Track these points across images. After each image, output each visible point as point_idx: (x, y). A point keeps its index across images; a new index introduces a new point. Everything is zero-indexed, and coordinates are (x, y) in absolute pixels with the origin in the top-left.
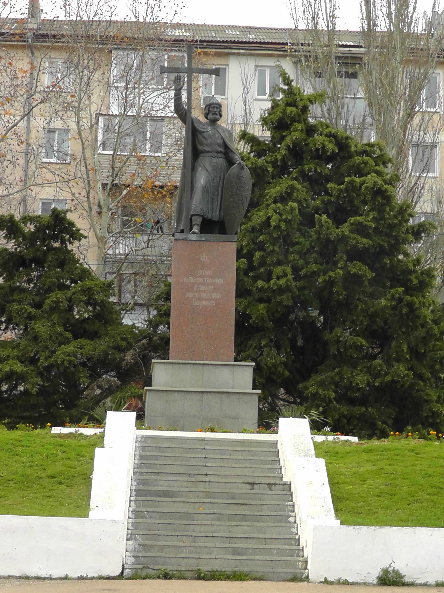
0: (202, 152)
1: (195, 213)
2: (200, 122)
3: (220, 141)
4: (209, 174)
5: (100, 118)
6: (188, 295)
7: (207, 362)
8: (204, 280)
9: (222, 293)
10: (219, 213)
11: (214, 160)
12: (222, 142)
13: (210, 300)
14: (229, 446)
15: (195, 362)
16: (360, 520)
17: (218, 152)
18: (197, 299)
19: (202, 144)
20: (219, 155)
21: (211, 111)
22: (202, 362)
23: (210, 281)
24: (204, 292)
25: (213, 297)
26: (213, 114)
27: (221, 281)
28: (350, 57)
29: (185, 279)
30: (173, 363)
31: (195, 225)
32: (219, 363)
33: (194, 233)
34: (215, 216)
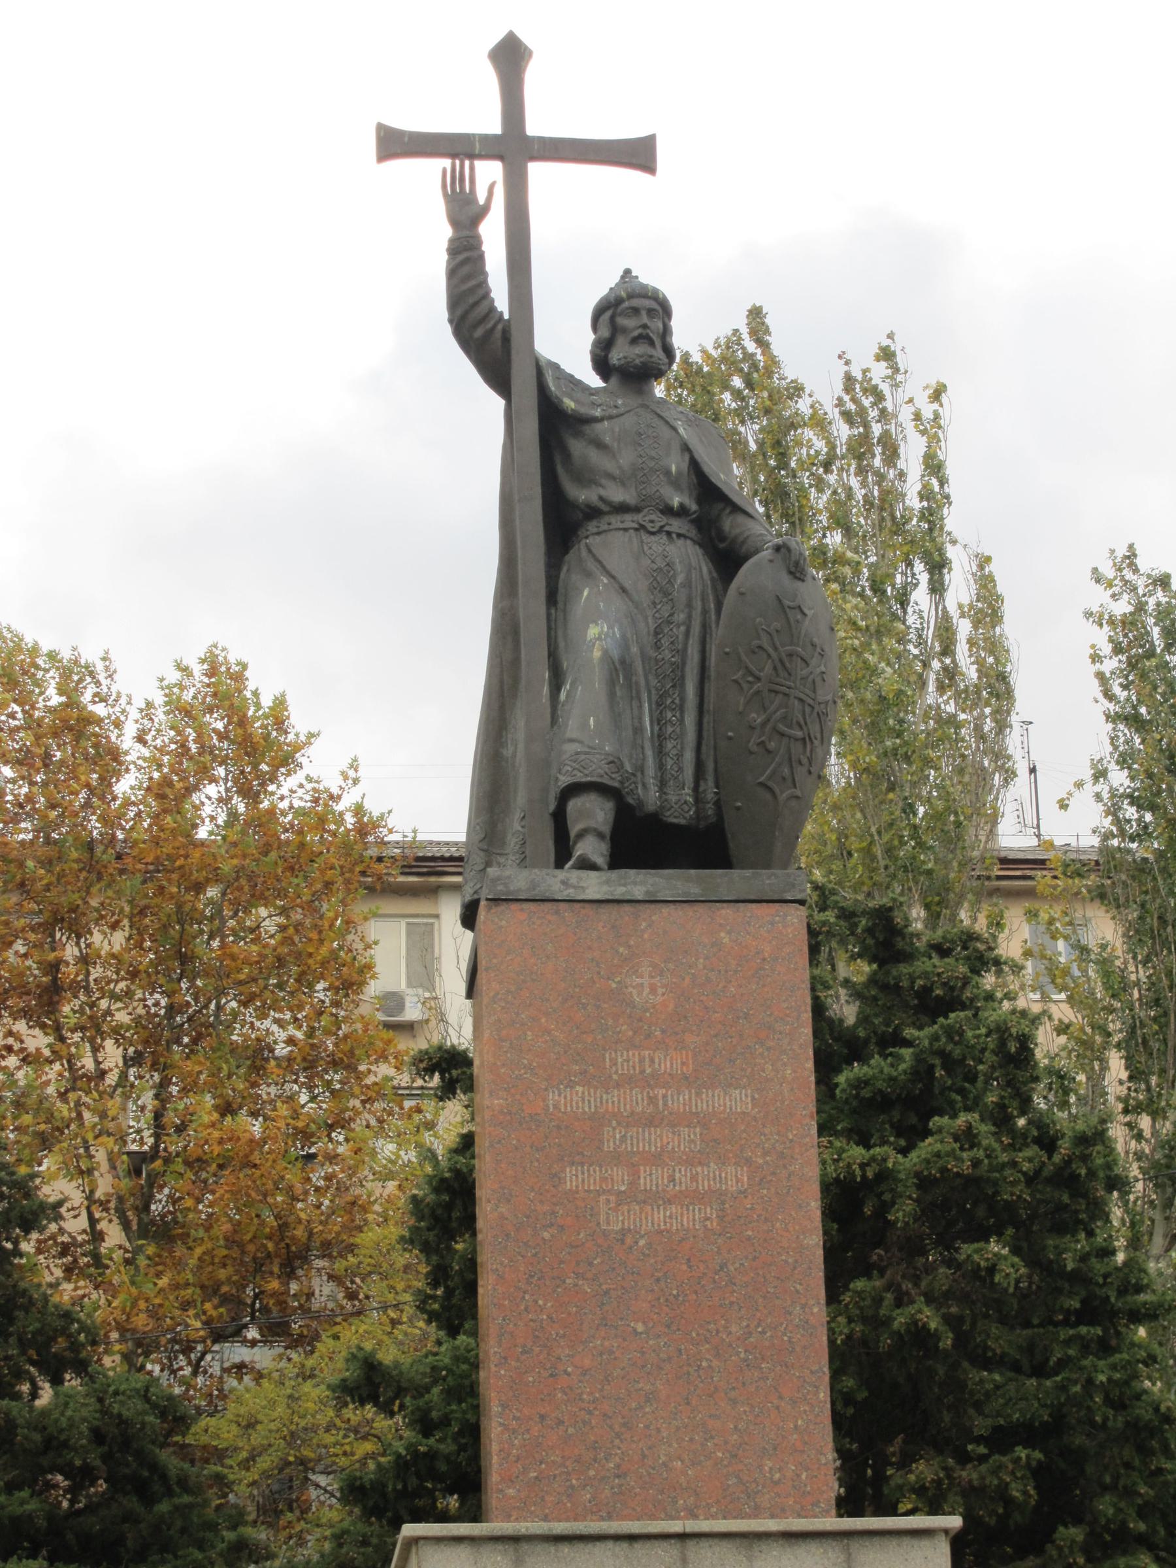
0: (593, 513)
1: (580, 777)
2: (575, 384)
3: (676, 464)
4: (637, 605)
6: (572, 1178)
7: (705, 1526)
8: (652, 1100)
9: (748, 1161)
10: (696, 788)
11: (657, 545)
12: (685, 466)
13: (696, 1197)
14: (567, 1520)
15: (635, 1527)
17: (668, 511)
18: (623, 1198)
19: (585, 478)
20: (676, 525)
21: (624, 330)
22: (676, 1527)
23: (680, 1101)
24: (656, 1159)
26: (634, 341)
27: (739, 1101)
29: (552, 1097)
30: (515, 1539)
31: (581, 835)
32: (772, 1525)
33: (586, 865)
34: (675, 800)
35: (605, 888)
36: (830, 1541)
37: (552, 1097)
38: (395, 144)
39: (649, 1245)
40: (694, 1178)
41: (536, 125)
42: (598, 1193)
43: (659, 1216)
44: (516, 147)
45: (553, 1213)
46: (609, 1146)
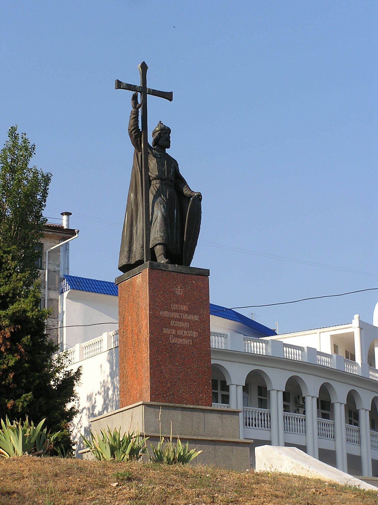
6: (165, 331)
7: (188, 406)
8: (180, 316)
9: (198, 331)
13: (187, 337)
23: (185, 316)
24: (181, 328)
25: (189, 335)
29: (161, 313)
37: (161, 313)
38: (119, 85)
39: (179, 347)
40: (188, 333)
41: (149, 86)
42: (170, 334)
44: (144, 90)
46: (172, 325)
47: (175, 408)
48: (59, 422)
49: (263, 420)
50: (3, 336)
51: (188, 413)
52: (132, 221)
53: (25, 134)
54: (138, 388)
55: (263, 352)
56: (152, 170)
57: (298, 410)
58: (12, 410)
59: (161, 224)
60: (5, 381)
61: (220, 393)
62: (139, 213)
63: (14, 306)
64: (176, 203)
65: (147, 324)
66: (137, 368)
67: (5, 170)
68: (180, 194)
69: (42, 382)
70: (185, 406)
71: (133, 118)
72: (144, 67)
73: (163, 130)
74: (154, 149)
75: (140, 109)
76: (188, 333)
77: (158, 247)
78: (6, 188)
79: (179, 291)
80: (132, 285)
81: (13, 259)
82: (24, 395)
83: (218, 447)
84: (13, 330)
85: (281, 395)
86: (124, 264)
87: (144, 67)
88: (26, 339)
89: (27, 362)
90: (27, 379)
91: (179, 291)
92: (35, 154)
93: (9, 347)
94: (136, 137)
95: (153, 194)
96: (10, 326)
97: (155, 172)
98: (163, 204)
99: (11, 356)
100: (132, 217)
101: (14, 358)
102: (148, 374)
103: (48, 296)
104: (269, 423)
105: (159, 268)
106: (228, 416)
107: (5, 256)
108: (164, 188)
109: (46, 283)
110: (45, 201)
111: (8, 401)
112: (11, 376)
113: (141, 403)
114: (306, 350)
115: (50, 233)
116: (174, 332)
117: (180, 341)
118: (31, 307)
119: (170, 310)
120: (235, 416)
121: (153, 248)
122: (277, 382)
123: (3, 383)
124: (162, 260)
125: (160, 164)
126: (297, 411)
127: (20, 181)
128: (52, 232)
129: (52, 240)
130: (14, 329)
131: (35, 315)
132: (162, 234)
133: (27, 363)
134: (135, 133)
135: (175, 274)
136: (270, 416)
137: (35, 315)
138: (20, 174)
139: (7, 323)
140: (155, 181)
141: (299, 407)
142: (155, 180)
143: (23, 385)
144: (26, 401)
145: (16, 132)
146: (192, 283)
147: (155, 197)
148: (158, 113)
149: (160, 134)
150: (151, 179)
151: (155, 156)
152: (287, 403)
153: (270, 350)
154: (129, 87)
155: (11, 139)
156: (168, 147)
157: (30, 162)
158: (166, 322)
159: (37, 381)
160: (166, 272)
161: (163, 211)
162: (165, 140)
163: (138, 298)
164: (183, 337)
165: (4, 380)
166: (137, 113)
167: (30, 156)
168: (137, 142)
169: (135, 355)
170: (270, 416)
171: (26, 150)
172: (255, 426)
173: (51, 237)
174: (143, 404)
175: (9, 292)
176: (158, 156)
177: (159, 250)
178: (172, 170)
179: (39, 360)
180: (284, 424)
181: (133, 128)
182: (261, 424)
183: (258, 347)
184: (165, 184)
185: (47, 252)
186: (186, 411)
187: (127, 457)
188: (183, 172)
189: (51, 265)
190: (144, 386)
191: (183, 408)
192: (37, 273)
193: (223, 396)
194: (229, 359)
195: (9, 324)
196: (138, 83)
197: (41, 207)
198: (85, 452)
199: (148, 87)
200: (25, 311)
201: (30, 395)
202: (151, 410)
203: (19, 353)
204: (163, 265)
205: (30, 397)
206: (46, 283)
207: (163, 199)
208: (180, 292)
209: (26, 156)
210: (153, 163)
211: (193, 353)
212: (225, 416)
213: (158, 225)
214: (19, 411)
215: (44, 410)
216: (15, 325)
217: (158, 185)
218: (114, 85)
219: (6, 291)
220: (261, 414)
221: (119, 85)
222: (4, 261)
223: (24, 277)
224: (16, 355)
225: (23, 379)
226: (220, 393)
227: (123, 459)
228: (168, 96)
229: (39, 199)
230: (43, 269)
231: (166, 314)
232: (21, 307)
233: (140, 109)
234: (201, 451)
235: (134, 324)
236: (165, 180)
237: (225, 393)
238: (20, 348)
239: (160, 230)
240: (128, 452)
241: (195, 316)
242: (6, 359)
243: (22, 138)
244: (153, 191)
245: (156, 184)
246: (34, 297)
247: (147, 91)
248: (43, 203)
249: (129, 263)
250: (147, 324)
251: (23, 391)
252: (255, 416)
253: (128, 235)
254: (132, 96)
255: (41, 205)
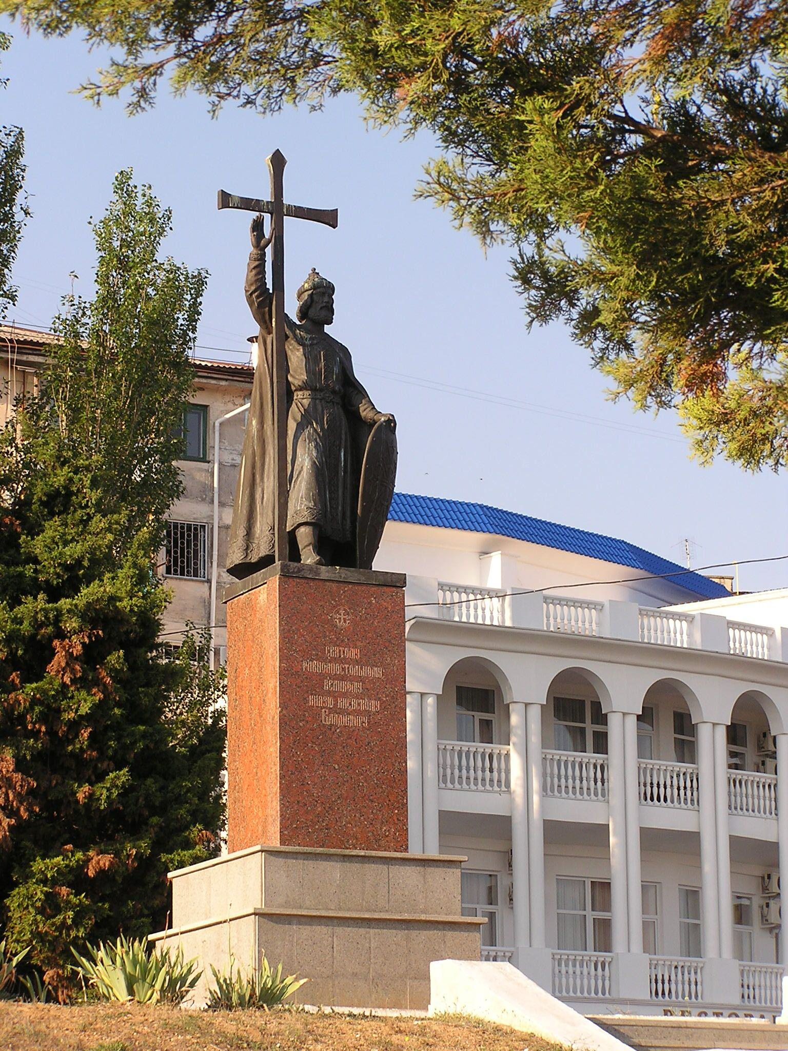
5: (189, 416)
6: (312, 701)
8: (343, 669)
13: (358, 713)
16: (381, 577)
23: (355, 670)
24: (344, 695)
28: (645, 910)
29: (305, 664)
35: (327, 574)
36: (311, 859)
37: (305, 664)
39: (341, 732)
40: (359, 704)
41: (288, 199)
43: (345, 719)
44: (278, 209)
45: (304, 715)
47: (328, 857)
48: (187, 827)
49: (682, 788)
50: (67, 652)
51: (356, 866)
52: (254, 475)
53: (150, 187)
54: (260, 814)
55: (682, 642)
56: (295, 371)
57: (763, 763)
58: (87, 806)
59: (309, 483)
60: (74, 745)
61: (590, 728)
62: (267, 460)
63: (90, 589)
64: (343, 437)
65: (275, 687)
66: (259, 774)
67: (108, 264)
68: (353, 416)
69: (152, 746)
70: (347, 852)
71: (254, 268)
72: (278, 161)
73: (318, 287)
74: (299, 327)
75: (268, 247)
76: (359, 704)
77: (302, 530)
78: (110, 303)
79: (342, 620)
80: (251, 606)
81: (94, 484)
82: (112, 775)
83: (414, 933)
84: (87, 640)
85: (721, 734)
86: (237, 562)
87: (278, 161)
88: (116, 658)
89: (119, 705)
90: (118, 739)
91: (342, 620)
92: (171, 229)
93: (79, 675)
94: (260, 305)
95: (295, 420)
96: (81, 631)
97: (302, 374)
98: (316, 440)
99: (83, 693)
100: (253, 467)
101: (90, 698)
102: (276, 788)
103: (220, 519)
104: (695, 793)
105: (300, 575)
106: (437, 870)
107: (76, 478)
108: (319, 408)
109: (216, 490)
110: (194, 330)
111: (80, 786)
112: (85, 735)
113: (258, 848)
114: (778, 634)
115: (223, 383)
116: (330, 702)
117: (344, 720)
118: (129, 588)
119: (323, 659)
120: (452, 870)
121: (294, 530)
122: (714, 705)
123: (70, 748)
124: (309, 557)
125: (310, 359)
126: (760, 767)
127: (139, 287)
128: (226, 380)
129: (227, 398)
130: (89, 637)
131: (136, 605)
132: (311, 504)
133: (119, 707)
134: (257, 297)
135: (334, 585)
136: (697, 779)
137: (136, 605)
138: (139, 273)
139: (74, 625)
140: (300, 393)
141: (767, 756)
142: (301, 390)
143: (110, 752)
144: (117, 786)
145: (131, 183)
146: (370, 603)
147: (300, 427)
148: (306, 253)
149: (311, 296)
150: (293, 388)
151: (301, 342)
152: (735, 748)
153: (698, 637)
154: (247, 204)
155: (120, 198)
156: (330, 322)
157: (159, 248)
158: (315, 684)
159: (141, 745)
160: (316, 582)
161: (315, 454)
162: (321, 308)
163: (261, 633)
164: (349, 712)
165: (71, 742)
166: (262, 258)
167: (160, 234)
168: (263, 314)
169: (255, 747)
170: (697, 779)
171: (152, 221)
172: (665, 800)
173: (224, 392)
174: (262, 851)
175: (83, 557)
176: (307, 342)
177: (304, 536)
178: (336, 370)
179: (146, 699)
180: (729, 795)
181: (253, 288)
182: (679, 795)
183: (680, 626)
184: (321, 400)
185: (217, 424)
186: (351, 862)
187: (156, 996)
188: (360, 374)
189: (226, 452)
190: (269, 811)
191: (344, 856)
192: (177, 486)
193: (595, 733)
194: (608, 657)
195: (80, 627)
196: (266, 195)
197: (186, 342)
198: (162, 938)
199: (286, 201)
200: (113, 599)
201: (123, 776)
202: (280, 861)
203: (101, 687)
204: (310, 568)
205: (123, 779)
206: (216, 490)
207: (315, 430)
208: (345, 622)
209: (150, 234)
210: (296, 356)
211: (369, 743)
212: (429, 870)
213: (304, 484)
214: (102, 807)
215: (157, 804)
216: (91, 630)
217: (306, 402)
218: (215, 200)
219: (76, 556)
220: (678, 775)
221: (226, 200)
222: (75, 489)
223: (117, 523)
224: (94, 690)
225: (110, 739)
226: (590, 728)
227: (149, 999)
228: (329, 218)
229: (182, 325)
230: (209, 462)
231: (313, 666)
232: (105, 590)
233: (268, 247)
234: (305, 980)
235: (253, 684)
236: (321, 390)
237: (599, 728)
238: (104, 677)
239: (308, 494)
240: (158, 986)
241: (375, 669)
242: (74, 701)
243: (144, 195)
244: (295, 414)
245: (302, 399)
246: (134, 568)
247: (285, 210)
248: (190, 334)
249: (248, 561)
250: (275, 687)
251: (112, 765)
252: (665, 778)
253: (246, 504)
254: (251, 222)
255: (186, 341)
